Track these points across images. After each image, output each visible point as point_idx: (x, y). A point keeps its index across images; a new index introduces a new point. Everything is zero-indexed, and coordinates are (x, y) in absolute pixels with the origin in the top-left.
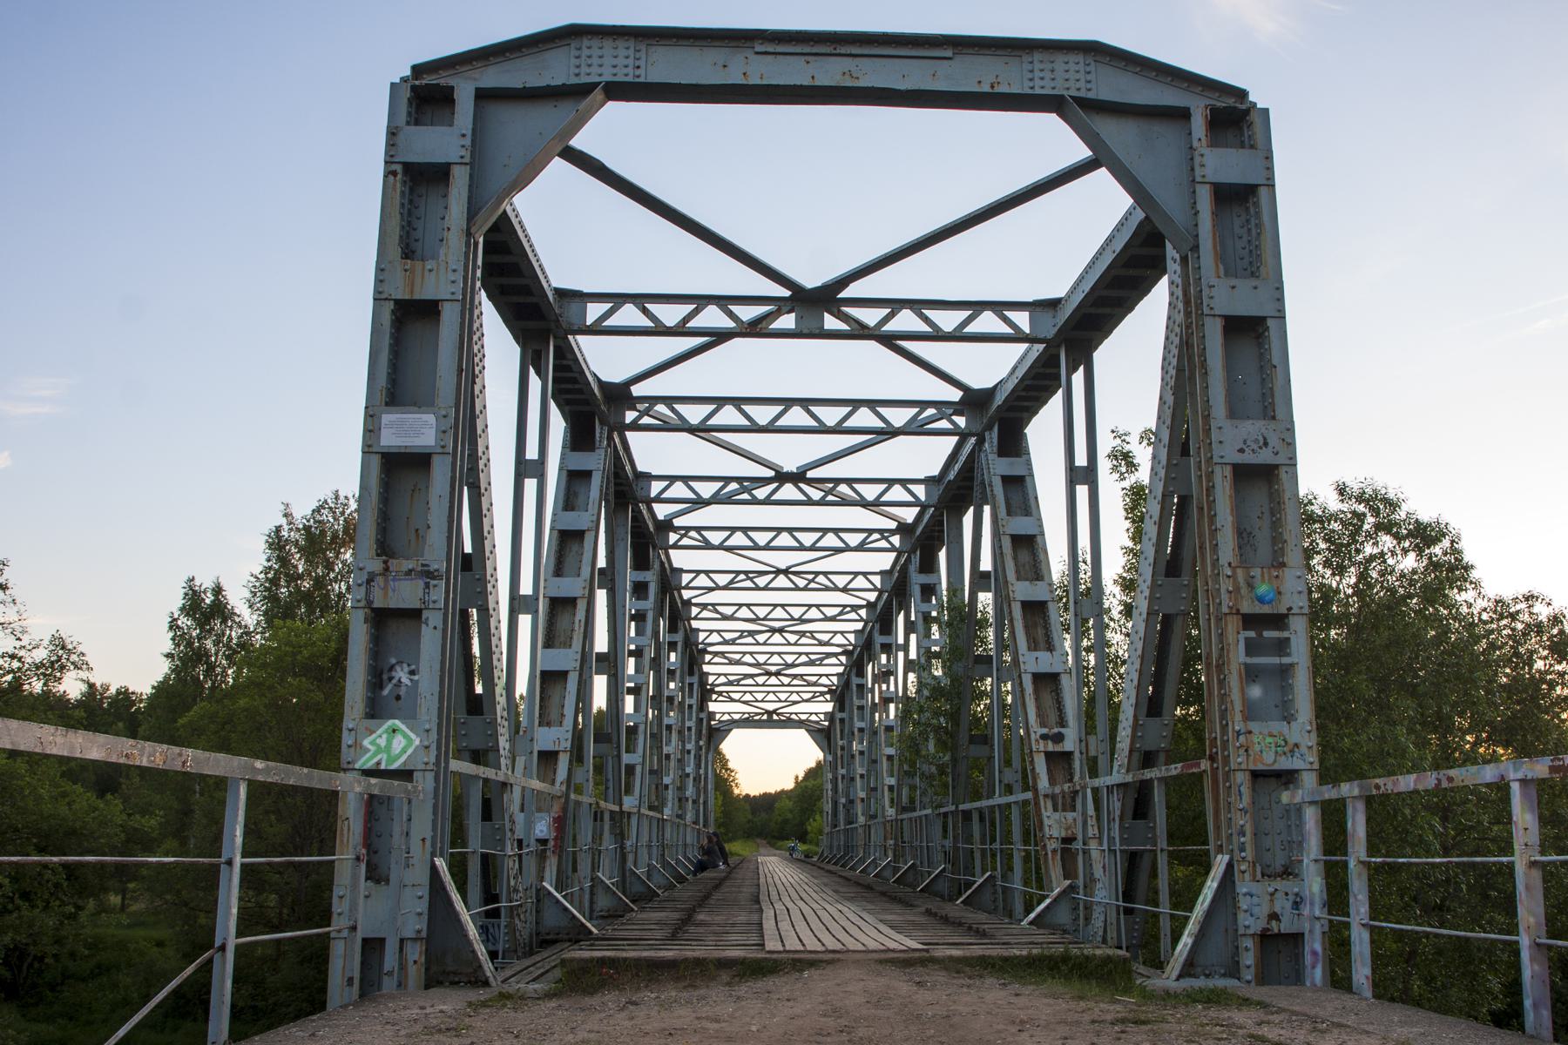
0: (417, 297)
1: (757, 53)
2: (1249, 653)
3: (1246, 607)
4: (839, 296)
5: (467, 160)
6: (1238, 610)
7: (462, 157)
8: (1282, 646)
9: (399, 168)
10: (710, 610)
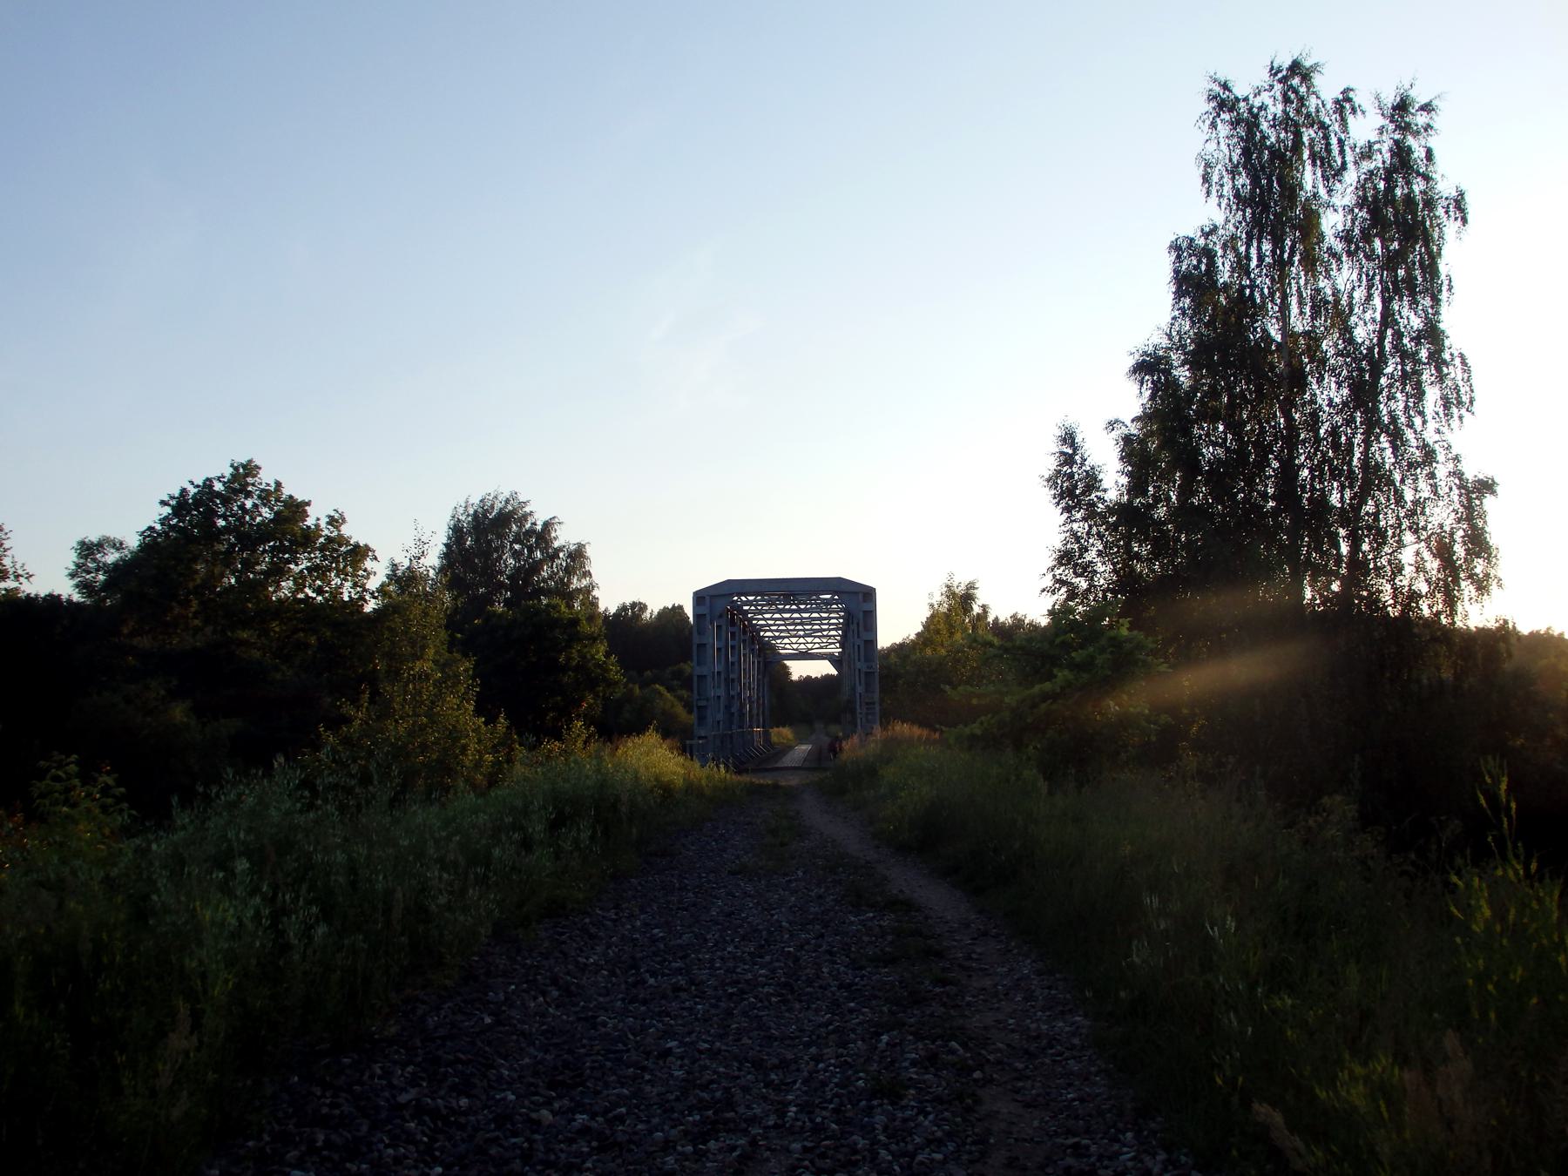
3: (867, 701)
8: (874, 708)
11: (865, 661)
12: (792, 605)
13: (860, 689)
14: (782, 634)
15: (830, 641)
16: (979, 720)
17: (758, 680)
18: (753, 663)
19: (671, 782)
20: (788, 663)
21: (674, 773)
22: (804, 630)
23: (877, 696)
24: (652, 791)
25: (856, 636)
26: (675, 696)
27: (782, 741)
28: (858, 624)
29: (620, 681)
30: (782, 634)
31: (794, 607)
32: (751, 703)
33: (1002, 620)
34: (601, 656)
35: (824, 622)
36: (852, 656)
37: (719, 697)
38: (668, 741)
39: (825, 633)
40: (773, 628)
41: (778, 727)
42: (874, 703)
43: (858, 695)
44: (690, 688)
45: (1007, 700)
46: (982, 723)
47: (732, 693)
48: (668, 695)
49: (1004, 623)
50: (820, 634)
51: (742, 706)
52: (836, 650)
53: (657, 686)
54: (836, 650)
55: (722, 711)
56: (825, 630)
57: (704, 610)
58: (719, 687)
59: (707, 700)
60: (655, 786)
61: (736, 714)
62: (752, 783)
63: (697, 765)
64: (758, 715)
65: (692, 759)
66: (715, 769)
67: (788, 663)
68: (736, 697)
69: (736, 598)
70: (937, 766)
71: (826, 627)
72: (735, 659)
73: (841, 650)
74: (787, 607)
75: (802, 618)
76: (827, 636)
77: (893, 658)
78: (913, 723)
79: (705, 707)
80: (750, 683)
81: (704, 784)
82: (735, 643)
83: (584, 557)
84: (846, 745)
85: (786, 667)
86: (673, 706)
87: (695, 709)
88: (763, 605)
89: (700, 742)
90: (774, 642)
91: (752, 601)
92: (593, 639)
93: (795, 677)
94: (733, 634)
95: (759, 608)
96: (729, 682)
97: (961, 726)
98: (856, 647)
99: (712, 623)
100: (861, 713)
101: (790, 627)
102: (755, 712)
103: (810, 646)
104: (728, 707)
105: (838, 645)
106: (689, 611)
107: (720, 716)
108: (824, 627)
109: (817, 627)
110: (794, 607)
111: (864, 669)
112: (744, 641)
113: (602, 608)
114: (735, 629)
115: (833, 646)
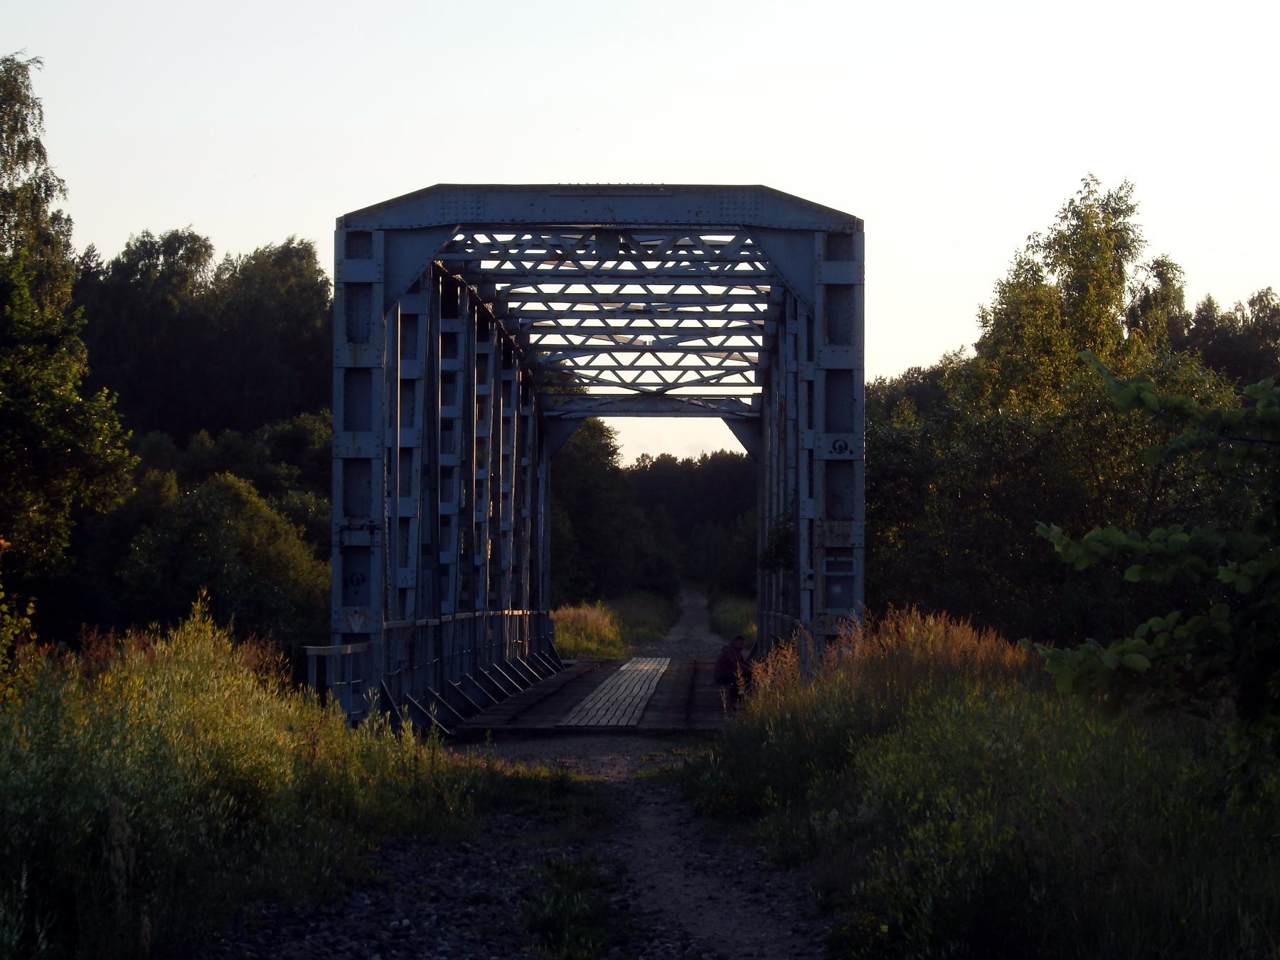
0: (358, 366)
1: (551, 196)
2: (828, 570)
3: (828, 544)
4: (636, 269)
5: (382, 281)
6: (823, 546)
7: (379, 279)
8: (849, 565)
9: (342, 285)
10: (586, 377)
11: (829, 429)
12: (621, 260)
13: (810, 508)
14: (592, 342)
15: (728, 363)
16: (1142, 629)
17: (521, 470)
18: (507, 421)
19: (261, 770)
20: (608, 422)
21: (271, 747)
22: (655, 330)
23: (857, 532)
24: (203, 798)
25: (803, 353)
26: (281, 509)
27: (585, 644)
28: (810, 321)
29: (119, 462)
30: (592, 342)
31: (628, 266)
32: (498, 537)
33: (1224, 307)
34: (68, 391)
35: (711, 309)
36: (792, 414)
37: (405, 521)
38: (244, 647)
39: (716, 341)
40: (564, 322)
41: (575, 603)
42: (849, 551)
43: (804, 526)
44: (325, 489)
45: (1224, 574)
46: (1150, 637)
47: (443, 508)
48: (262, 503)
49: (1230, 319)
50: (700, 343)
51: (472, 547)
52: (744, 388)
53: (231, 478)
54: (744, 388)
55: (412, 563)
56: (715, 332)
57: (368, 271)
58: (406, 491)
59: (372, 529)
60: (214, 784)
61: (452, 570)
62: (492, 775)
63: (338, 718)
64: (517, 570)
65: (323, 702)
66: (389, 734)
67: (608, 422)
68: (454, 521)
69: (460, 237)
70: (1018, 748)
71: (719, 323)
72: (456, 412)
73: (759, 390)
74: (609, 265)
75: (649, 297)
76: (720, 349)
77: (908, 421)
78: (956, 614)
79: (366, 550)
80: (495, 480)
81: (356, 780)
82: (457, 364)
83: (24, 101)
84: (763, 675)
85: (604, 432)
86: (274, 536)
87: (336, 551)
88: (539, 260)
89: (349, 649)
90: (569, 363)
91: (506, 245)
92: (50, 342)
93: (627, 459)
94: (450, 339)
95: (528, 265)
96: (435, 477)
97: (1091, 644)
98: (803, 388)
99: (389, 307)
100: (811, 577)
101: (614, 323)
102: (509, 560)
103: (670, 376)
104: (430, 550)
105: (751, 375)
106: (326, 262)
107: (407, 576)
108: (712, 323)
109: (694, 323)
110: (628, 266)
111: (824, 453)
112: (483, 358)
113: (78, 248)
114: (456, 326)
115: (737, 378)
